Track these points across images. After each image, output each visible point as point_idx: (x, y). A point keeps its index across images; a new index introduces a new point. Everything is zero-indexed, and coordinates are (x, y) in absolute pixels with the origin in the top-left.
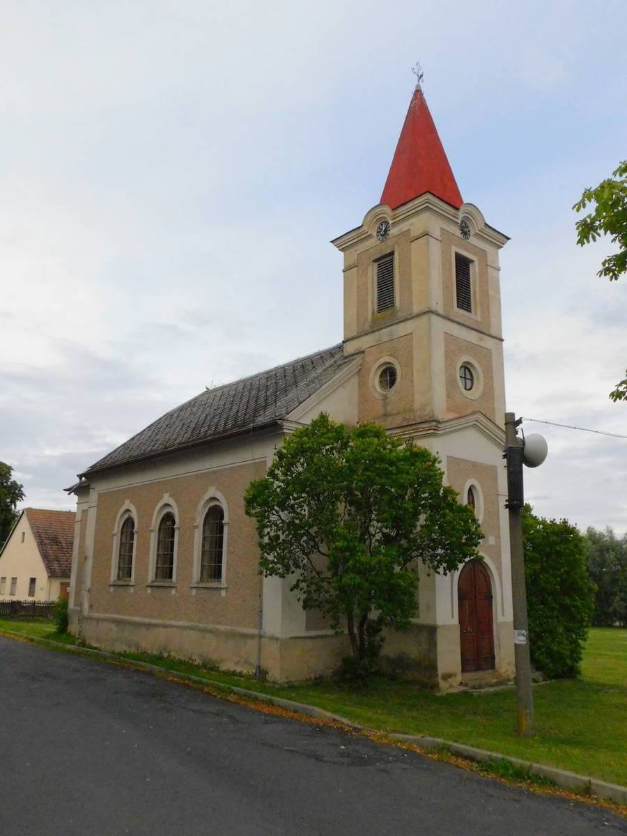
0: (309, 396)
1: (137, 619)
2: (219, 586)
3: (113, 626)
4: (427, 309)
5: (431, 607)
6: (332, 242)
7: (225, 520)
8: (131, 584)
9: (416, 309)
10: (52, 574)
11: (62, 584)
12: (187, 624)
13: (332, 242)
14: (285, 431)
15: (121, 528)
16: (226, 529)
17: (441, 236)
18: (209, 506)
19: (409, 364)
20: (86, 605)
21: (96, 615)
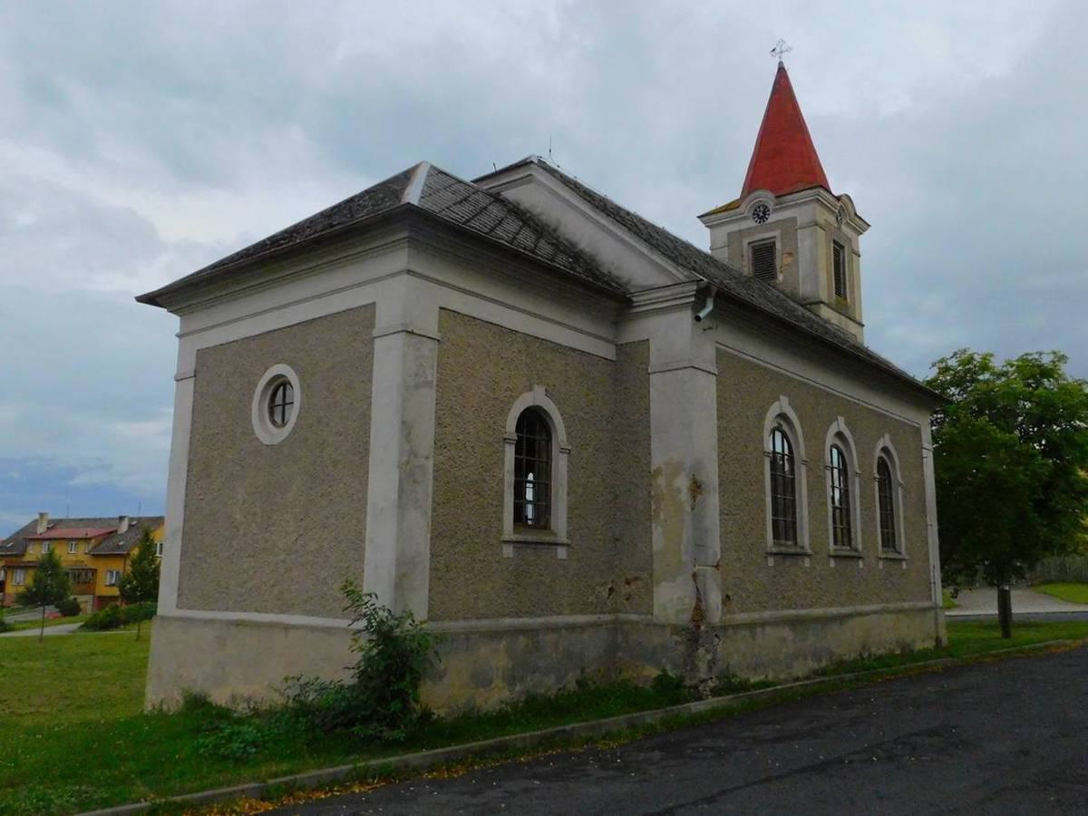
1: (818, 611)
3: (787, 632)
6: (699, 217)
13: (699, 217)
20: (714, 598)
21: (741, 617)
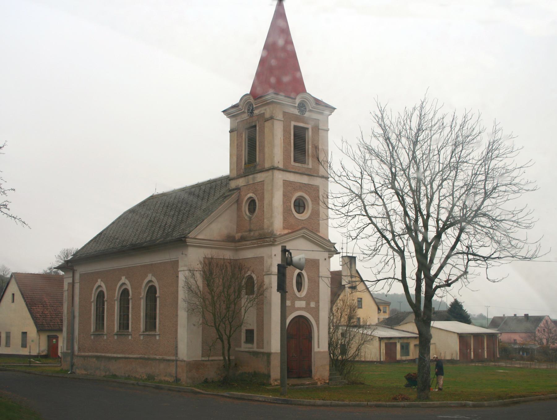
0: (196, 227)
2: (155, 333)
4: (272, 167)
5: (269, 343)
7: (158, 295)
8: (104, 333)
9: (267, 165)
10: (40, 329)
11: (48, 336)
12: (139, 356)
14: (188, 244)
15: (96, 297)
16: (158, 300)
17: (283, 117)
18: (149, 286)
19: (262, 199)
